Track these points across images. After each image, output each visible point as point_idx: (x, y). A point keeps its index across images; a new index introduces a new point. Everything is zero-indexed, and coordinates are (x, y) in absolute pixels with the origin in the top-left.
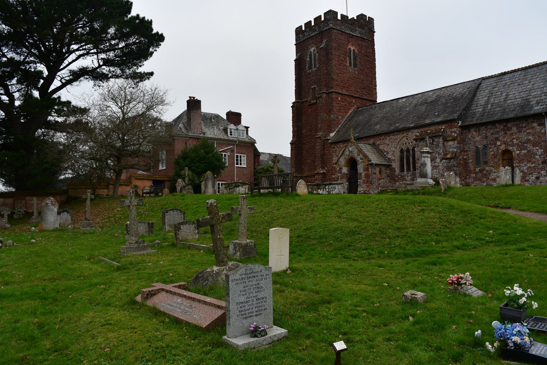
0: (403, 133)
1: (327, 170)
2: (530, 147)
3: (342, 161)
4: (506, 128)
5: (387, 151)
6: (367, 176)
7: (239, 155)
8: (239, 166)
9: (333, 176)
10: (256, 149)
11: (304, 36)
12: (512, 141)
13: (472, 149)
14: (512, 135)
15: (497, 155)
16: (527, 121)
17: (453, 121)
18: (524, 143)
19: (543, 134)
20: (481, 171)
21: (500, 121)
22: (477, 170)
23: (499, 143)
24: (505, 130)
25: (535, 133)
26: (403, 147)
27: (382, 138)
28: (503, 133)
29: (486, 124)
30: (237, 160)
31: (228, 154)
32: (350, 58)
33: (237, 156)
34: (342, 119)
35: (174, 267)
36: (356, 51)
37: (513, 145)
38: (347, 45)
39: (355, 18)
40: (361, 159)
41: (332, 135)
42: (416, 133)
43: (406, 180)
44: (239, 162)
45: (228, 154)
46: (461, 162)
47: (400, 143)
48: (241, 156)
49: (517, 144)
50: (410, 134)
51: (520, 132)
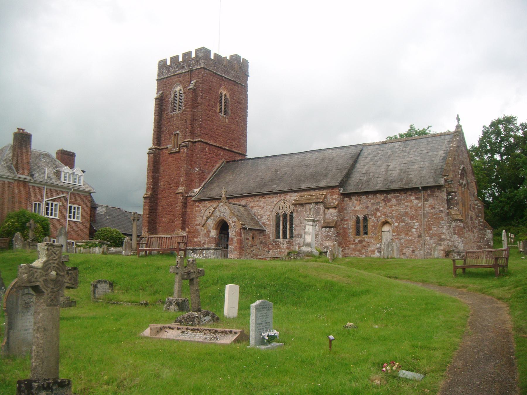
0: (280, 196)
1: (188, 232)
2: (407, 219)
3: (211, 223)
4: (386, 199)
5: (260, 215)
6: (240, 242)
7: (73, 206)
8: (72, 219)
9: (196, 240)
10: (92, 201)
11: (169, 71)
12: (391, 213)
13: (353, 218)
14: (391, 206)
15: (377, 226)
16: (405, 193)
17: (333, 187)
18: (403, 216)
19: (419, 207)
20: (361, 242)
21: (381, 192)
22: (357, 241)
23: (379, 214)
24: (385, 201)
25: (413, 206)
26: (280, 212)
27: (255, 200)
28: (383, 204)
29: (367, 193)
30: (70, 212)
31: (59, 204)
32: (221, 103)
33: (70, 208)
34: (209, 173)
35: (490, 250)
36: (228, 97)
37: (392, 217)
38: (219, 89)
39: (228, 58)
40: (233, 222)
41: (197, 190)
42: (293, 197)
43: (281, 248)
44: (50, 212)
45: (59, 204)
46: (341, 231)
47: (276, 207)
48: (75, 208)
49: (396, 216)
50: (288, 198)
51: (399, 204)
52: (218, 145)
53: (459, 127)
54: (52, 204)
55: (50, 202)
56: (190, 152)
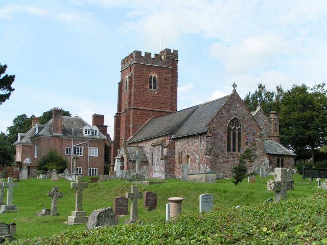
31: (83, 147)
36: (157, 77)
45: (83, 147)
52: (149, 109)
53: (235, 91)
54: (78, 148)
55: (77, 147)
56: (128, 115)
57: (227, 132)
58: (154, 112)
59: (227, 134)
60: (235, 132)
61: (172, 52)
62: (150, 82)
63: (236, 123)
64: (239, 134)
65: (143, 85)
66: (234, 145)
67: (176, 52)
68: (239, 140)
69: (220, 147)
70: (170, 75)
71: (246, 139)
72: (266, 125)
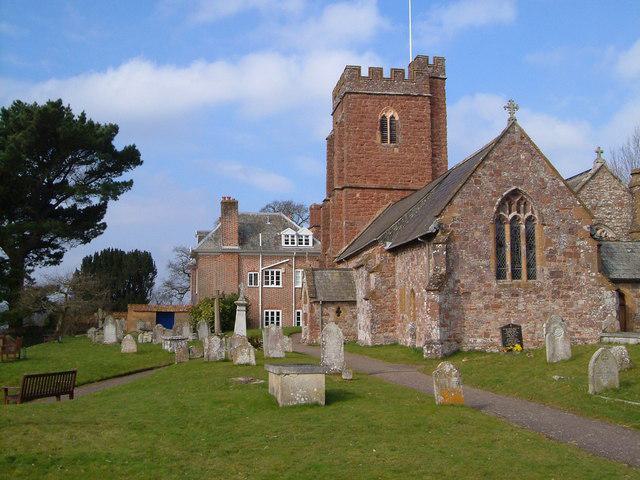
31: (282, 271)
36: (397, 118)
53: (513, 123)
57: (492, 229)
58: (392, 193)
59: (492, 235)
60: (519, 228)
61: (431, 62)
62: (383, 129)
63: (518, 203)
64: (530, 237)
65: (368, 138)
66: (515, 261)
67: (440, 61)
68: (530, 247)
69: (474, 269)
70: (427, 111)
71: (549, 242)
72: (621, 204)
